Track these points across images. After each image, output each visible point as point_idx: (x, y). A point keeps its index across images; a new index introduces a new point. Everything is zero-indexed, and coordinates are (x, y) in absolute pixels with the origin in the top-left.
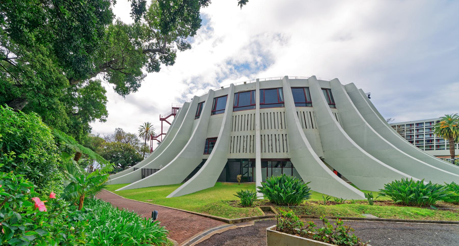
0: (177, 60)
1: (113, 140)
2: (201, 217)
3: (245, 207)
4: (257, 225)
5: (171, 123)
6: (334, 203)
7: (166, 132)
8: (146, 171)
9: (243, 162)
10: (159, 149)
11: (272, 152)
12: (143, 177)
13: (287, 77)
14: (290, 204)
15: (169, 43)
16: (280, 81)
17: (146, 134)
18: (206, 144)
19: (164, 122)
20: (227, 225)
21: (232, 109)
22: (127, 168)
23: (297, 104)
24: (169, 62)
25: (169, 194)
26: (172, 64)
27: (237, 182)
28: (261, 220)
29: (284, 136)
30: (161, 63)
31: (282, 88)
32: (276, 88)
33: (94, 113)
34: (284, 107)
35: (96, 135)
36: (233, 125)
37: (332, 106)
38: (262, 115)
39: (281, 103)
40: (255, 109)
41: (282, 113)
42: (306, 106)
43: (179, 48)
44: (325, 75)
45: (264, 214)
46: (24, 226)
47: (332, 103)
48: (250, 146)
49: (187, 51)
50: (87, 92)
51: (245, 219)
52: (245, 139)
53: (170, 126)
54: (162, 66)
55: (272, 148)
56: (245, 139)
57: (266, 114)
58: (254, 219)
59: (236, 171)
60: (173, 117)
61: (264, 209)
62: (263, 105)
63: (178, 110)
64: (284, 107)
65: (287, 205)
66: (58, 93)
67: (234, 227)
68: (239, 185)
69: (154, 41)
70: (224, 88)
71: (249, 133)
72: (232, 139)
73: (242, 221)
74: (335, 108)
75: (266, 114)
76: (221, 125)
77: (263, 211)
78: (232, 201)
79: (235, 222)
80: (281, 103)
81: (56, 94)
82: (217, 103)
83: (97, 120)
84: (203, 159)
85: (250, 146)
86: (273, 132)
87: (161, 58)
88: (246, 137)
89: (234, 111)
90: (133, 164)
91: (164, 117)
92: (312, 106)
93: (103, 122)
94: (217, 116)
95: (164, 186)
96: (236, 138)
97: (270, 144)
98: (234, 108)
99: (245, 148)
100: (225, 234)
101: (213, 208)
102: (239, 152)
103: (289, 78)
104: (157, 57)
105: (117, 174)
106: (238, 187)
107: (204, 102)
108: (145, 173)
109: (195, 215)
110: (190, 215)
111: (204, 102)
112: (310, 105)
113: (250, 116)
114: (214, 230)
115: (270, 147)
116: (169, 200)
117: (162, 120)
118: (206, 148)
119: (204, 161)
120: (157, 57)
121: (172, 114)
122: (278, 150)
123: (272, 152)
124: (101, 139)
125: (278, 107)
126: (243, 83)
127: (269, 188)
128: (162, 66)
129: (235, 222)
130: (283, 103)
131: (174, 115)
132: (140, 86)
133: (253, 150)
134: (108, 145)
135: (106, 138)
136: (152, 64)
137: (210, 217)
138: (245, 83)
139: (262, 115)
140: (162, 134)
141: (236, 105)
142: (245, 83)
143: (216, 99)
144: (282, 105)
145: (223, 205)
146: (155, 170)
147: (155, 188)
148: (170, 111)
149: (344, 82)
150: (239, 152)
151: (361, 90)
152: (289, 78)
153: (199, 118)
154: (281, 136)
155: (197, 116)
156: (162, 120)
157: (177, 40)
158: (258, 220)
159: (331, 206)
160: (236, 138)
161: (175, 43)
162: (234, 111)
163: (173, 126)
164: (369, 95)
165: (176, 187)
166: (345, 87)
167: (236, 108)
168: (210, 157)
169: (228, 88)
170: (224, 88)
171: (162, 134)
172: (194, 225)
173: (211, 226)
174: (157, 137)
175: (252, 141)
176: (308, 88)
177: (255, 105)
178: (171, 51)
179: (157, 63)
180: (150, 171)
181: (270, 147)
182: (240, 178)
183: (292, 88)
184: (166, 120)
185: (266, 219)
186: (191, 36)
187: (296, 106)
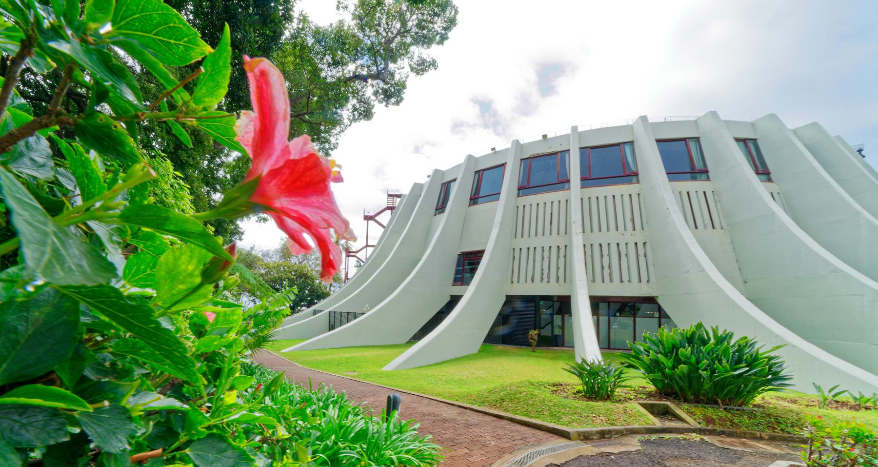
0: (406, 94)
1: (276, 259)
2: (488, 419)
3: (597, 401)
4: (650, 449)
5: (385, 225)
6: (856, 408)
7: (375, 243)
8: (338, 315)
9: (542, 303)
10: (361, 277)
11: (611, 281)
12: (332, 327)
13: (644, 119)
14: (723, 401)
15: (395, 62)
16: (628, 128)
18: (458, 265)
19: (371, 222)
20: (563, 442)
21: (516, 191)
22: (299, 311)
23: (673, 174)
24: (393, 100)
25: (386, 362)
26: (398, 103)
27: (529, 345)
28: (654, 437)
29: (640, 246)
30: (376, 103)
31: (632, 143)
32: (618, 144)
34: (638, 182)
35: (248, 248)
36: (517, 225)
37: (764, 177)
39: (629, 175)
40: (569, 189)
42: (694, 179)
43: (412, 69)
44: (743, 111)
45: (656, 422)
46: (125, 415)
47: (763, 171)
48: (558, 268)
49: (431, 73)
50: (239, 167)
51: (610, 432)
52: (546, 254)
53: (382, 230)
54: (379, 108)
55: (610, 274)
56: (546, 254)
57: (594, 201)
58: (633, 432)
59: (529, 323)
60: (389, 212)
61: (651, 408)
62: (587, 180)
63: (398, 200)
64: (638, 182)
65: (716, 403)
66: (194, 159)
67: (588, 449)
68: (533, 351)
69: (365, 60)
70: (497, 150)
71: (555, 241)
72: (514, 255)
73: (603, 435)
74: (770, 180)
75: (594, 201)
76: (491, 227)
77: (652, 413)
78: (554, 385)
79: (586, 437)
80: (629, 175)
81: (191, 162)
82: (482, 182)
83: (254, 218)
84: (452, 296)
85: (558, 268)
86: (613, 237)
87: (376, 93)
88: (547, 249)
89: (518, 196)
90: (310, 304)
91: (372, 214)
92: (708, 179)
93: (262, 223)
94: (482, 207)
95: (373, 346)
96: (524, 251)
98: (519, 189)
99: (546, 272)
101: (509, 397)
102: (533, 281)
103: (650, 121)
104: (369, 92)
106: (532, 356)
107: (455, 180)
108: (334, 321)
109: (470, 412)
110: (458, 410)
111: (455, 180)
112: (704, 176)
113: (556, 204)
114: (539, 453)
115: (606, 271)
116: (388, 375)
117: (367, 218)
118: (457, 272)
119: (454, 301)
120: (369, 92)
121: (388, 208)
122: (625, 277)
123: (611, 281)
124: (256, 257)
125: (623, 183)
126: (541, 138)
127: (661, 358)
128: (379, 108)
129: (586, 437)
130: (636, 174)
131: (391, 208)
132: (336, 148)
133: (567, 276)
134: (267, 267)
135: (264, 255)
136: (358, 106)
137: (512, 420)
138: (545, 137)
139: (586, 202)
140: (367, 246)
141: (526, 184)
142: (545, 137)
143: (479, 173)
144: (634, 179)
145: (536, 392)
146: (356, 315)
147: (355, 350)
148: (384, 202)
149: (792, 122)
150: (533, 281)
151: (839, 138)
152: (650, 121)
153: (443, 212)
154: (632, 247)
155: (441, 208)
156: (367, 218)
157: (409, 55)
158: (646, 437)
159: (846, 413)
160: (524, 251)
161: (406, 60)
162: (518, 196)
163: (390, 231)
164: (860, 151)
165: (402, 350)
166: (795, 132)
167: (524, 189)
168: (469, 292)
169: (507, 150)
170: (497, 150)
171: (367, 246)
172: (480, 436)
173: (526, 443)
174: (357, 252)
175: (562, 260)
176: (697, 139)
177: (568, 181)
178: (397, 77)
179: (369, 104)
180: (345, 316)
181: (606, 271)
182: (536, 338)
183: (658, 141)
184: (377, 218)
185: (667, 436)
186: (439, 43)
187: (670, 180)
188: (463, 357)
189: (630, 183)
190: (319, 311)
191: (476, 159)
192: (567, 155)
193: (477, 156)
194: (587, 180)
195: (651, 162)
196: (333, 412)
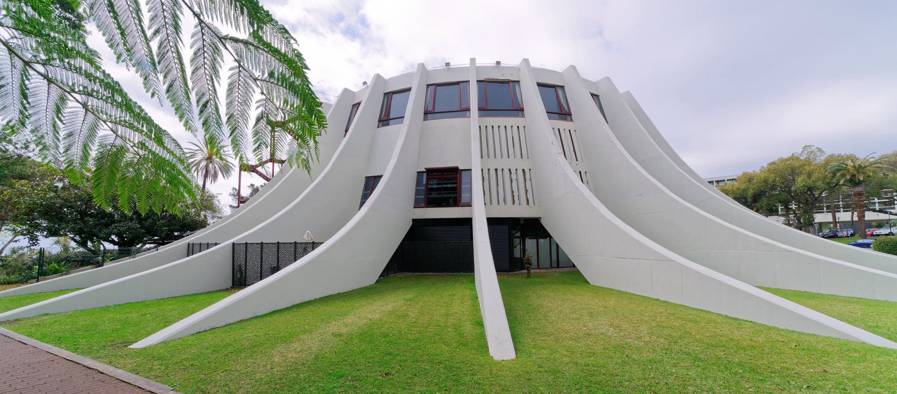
17: (207, 166)
32: (458, 83)
33: (805, 220)
34: (523, 116)
38: (483, 129)
39: (518, 110)
41: (521, 129)
48: (526, 191)
52: (514, 176)
57: (490, 128)
75: (490, 128)
85: (526, 191)
92: (572, 120)
97: (514, 182)
100: (612, 302)
105: (108, 265)
130: (522, 110)
139: (483, 129)
143: (388, 95)
144: (520, 113)
177: (468, 110)
188: (292, 307)
189: (517, 116)
190: (201, 247)
191: (386, 80)
192: (517, 86)
193: (386, 78)
194: (483, 110)
195: (533, 101)
196: (710, 382)
